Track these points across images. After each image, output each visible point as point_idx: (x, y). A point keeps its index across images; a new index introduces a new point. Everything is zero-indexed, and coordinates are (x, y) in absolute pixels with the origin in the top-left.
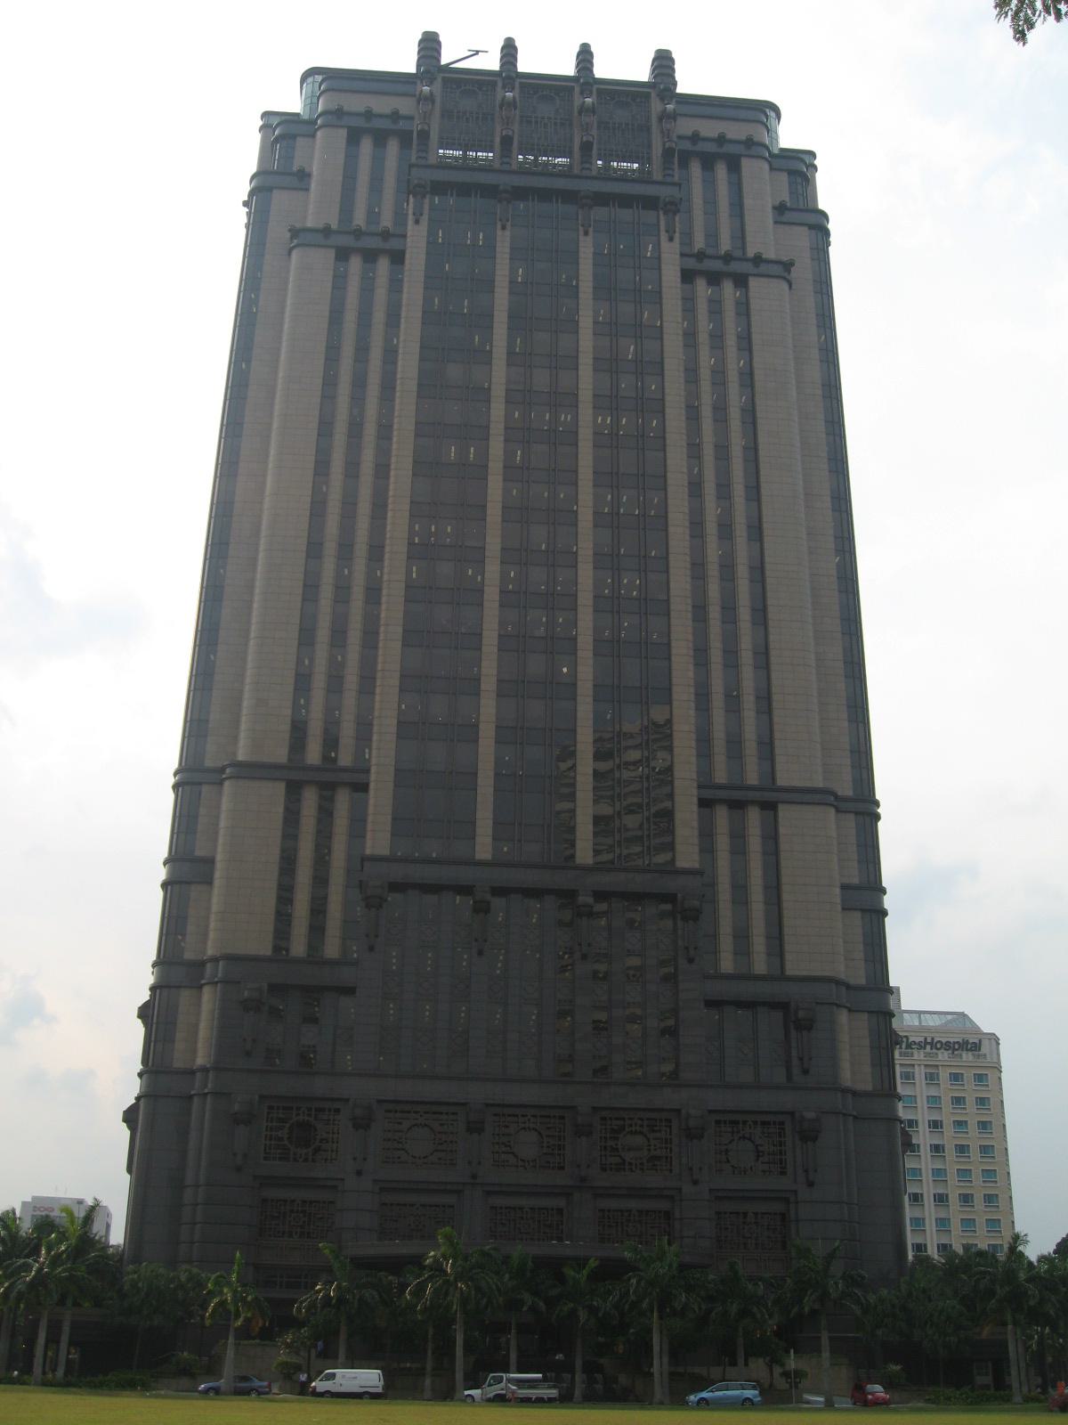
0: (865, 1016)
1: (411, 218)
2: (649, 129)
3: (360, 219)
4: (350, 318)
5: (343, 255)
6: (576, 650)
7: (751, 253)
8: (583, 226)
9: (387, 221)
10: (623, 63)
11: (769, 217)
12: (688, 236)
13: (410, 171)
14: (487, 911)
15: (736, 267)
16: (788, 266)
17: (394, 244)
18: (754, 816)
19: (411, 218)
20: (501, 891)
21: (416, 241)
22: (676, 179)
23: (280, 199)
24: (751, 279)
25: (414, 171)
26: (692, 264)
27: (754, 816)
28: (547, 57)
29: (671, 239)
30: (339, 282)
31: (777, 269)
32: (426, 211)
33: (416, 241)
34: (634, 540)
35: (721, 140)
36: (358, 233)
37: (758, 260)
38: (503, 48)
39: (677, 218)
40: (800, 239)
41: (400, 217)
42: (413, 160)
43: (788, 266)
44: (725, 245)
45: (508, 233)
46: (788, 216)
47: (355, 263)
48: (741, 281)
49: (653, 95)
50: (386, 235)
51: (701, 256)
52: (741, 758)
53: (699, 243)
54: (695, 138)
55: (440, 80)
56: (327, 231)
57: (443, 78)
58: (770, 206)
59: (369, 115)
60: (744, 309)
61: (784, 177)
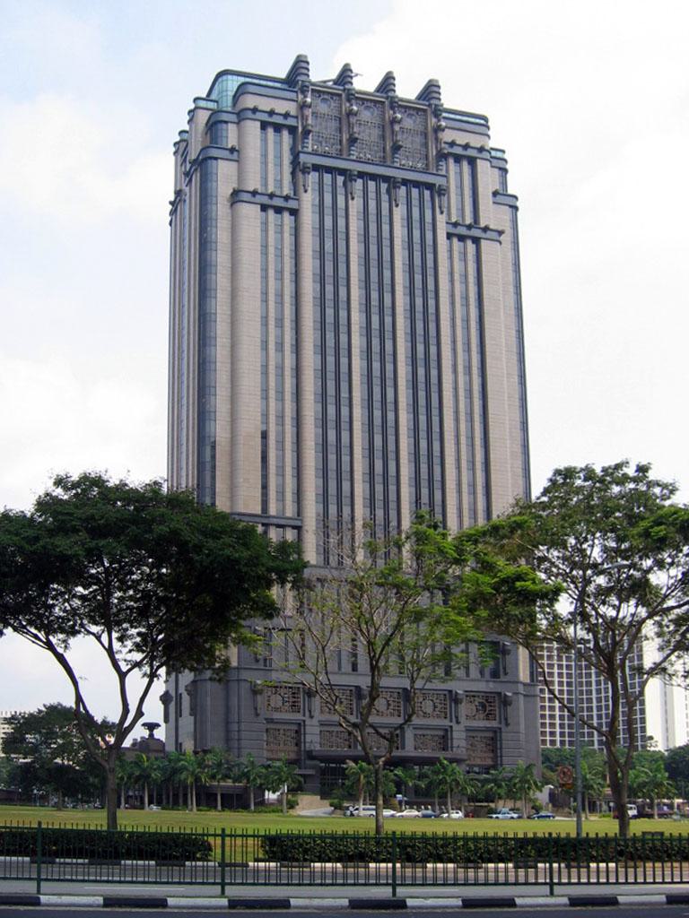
9: (287, 190)
12: (449, 215)
15: (476, 233)
16: (501, 233)
17: (292, 204)
29: (306, 191)
31: (494, 235)
37: (486, 229)
51: (455, 225)
56: (254, 193)
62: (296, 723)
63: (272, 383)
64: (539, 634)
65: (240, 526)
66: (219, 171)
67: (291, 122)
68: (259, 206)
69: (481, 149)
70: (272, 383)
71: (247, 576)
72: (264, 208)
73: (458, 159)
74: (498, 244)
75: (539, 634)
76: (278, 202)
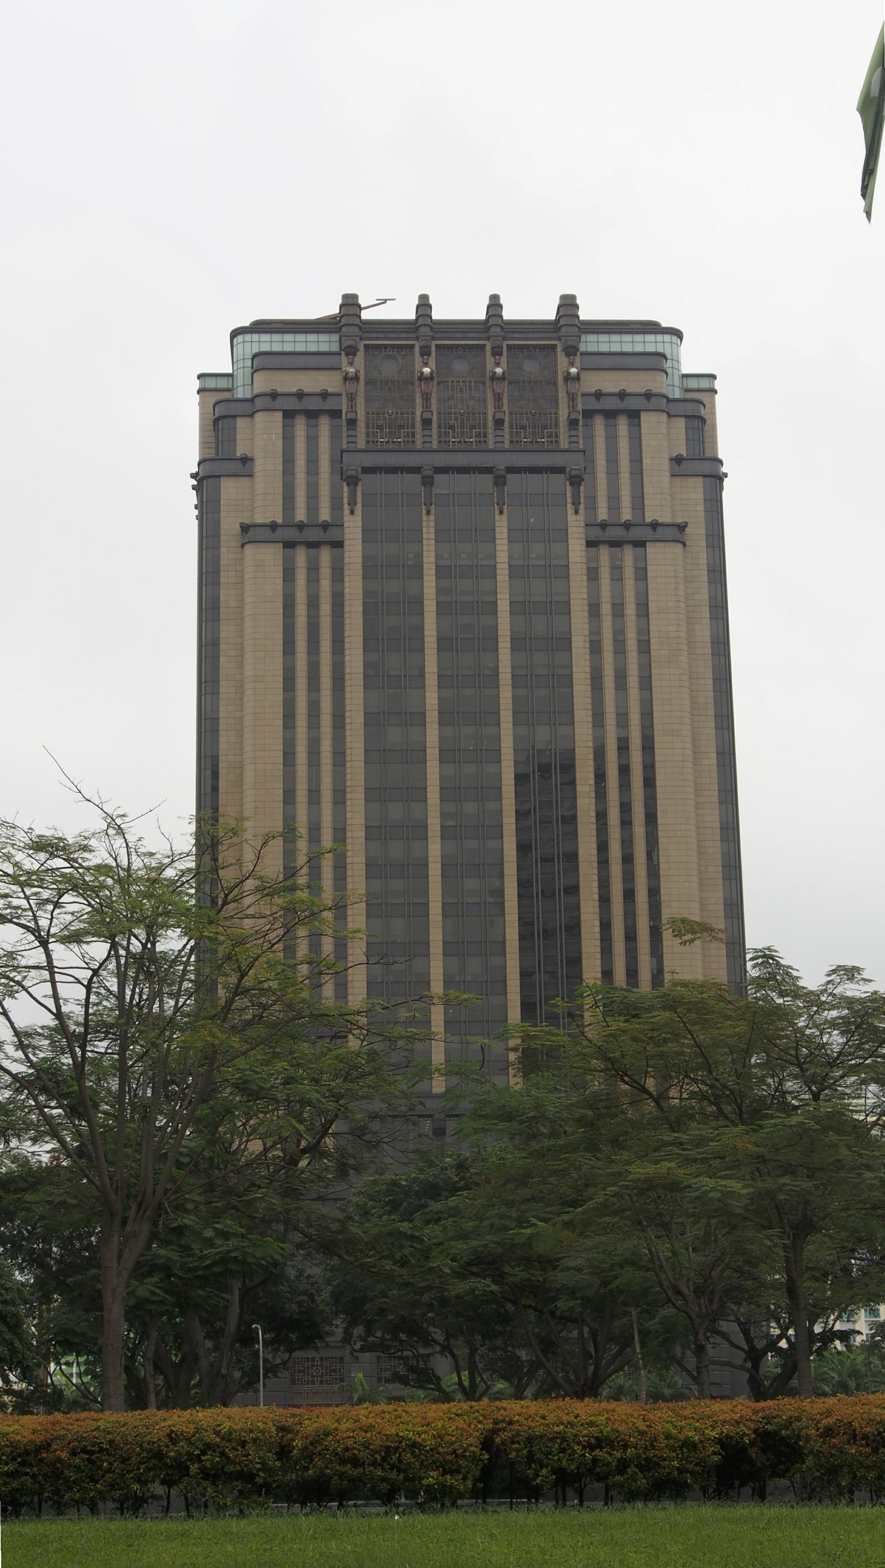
0: (701, 479)
1: (346, 507)
2: (555, 384)
3: (301, 515)
4: (301, 610)
5: (289, 415)
6: (496, 575)
7: (648, 520)
8: (498, 504)
9: (325, 515)
10: (531, 305)
11: (666, 465)
12: (592, 507)
13: (342, 457)
14: (432, 484)
15: (636, 533)
16: (682, 528)
17: (332, 534)
18: (623, 426)
19: (346, 507)
20: (439, 470)
21: (353, 528)
22: (581, 446)
23: (229, 489)
24: (642, 413)
25: (346, 456)
26: (596, 533)
27: (623, 426)
28: (458, 305)
30: (288, 439)
31: (670, 533)
32: (359, 500)
33: (353, 528)
34: (545, 691)
35: (622, 395)
36: (301, 526)
37: (655, 525)
38: (418, 307)
39: (582, 488)
40: (694, 491)
41: (336, 505)
42: (344, 446)
43: (682, 528)
44: (626, 515)
45: (432, 518)
46: (685, 465)
47: (300, 426)
48: (634, 415)
49: (559, 349)
50: (325, 526)
51: (603, 526)
52: (625, 653)
53: (603, 515)
54: (598, 395)
55: (362, 348)
56: (273, 526)
57: (366, 347)
58: (667, 456)
59: (300, 395)
60: (642, 574)
61: (681, 423)
62: (331, 1347)
63: (325, 584)
64: (65, 1067)
65: (367, 1388)
66: (223, 496)
67: (330, 404)
68: (281, 545)
69: (648, 395)
70: (325, 584)
71: (162, 1253)
72: (289, 545)
73: (610, 415)
74: (680, 546)
75: (65, 1067)
76: (313, 535)
